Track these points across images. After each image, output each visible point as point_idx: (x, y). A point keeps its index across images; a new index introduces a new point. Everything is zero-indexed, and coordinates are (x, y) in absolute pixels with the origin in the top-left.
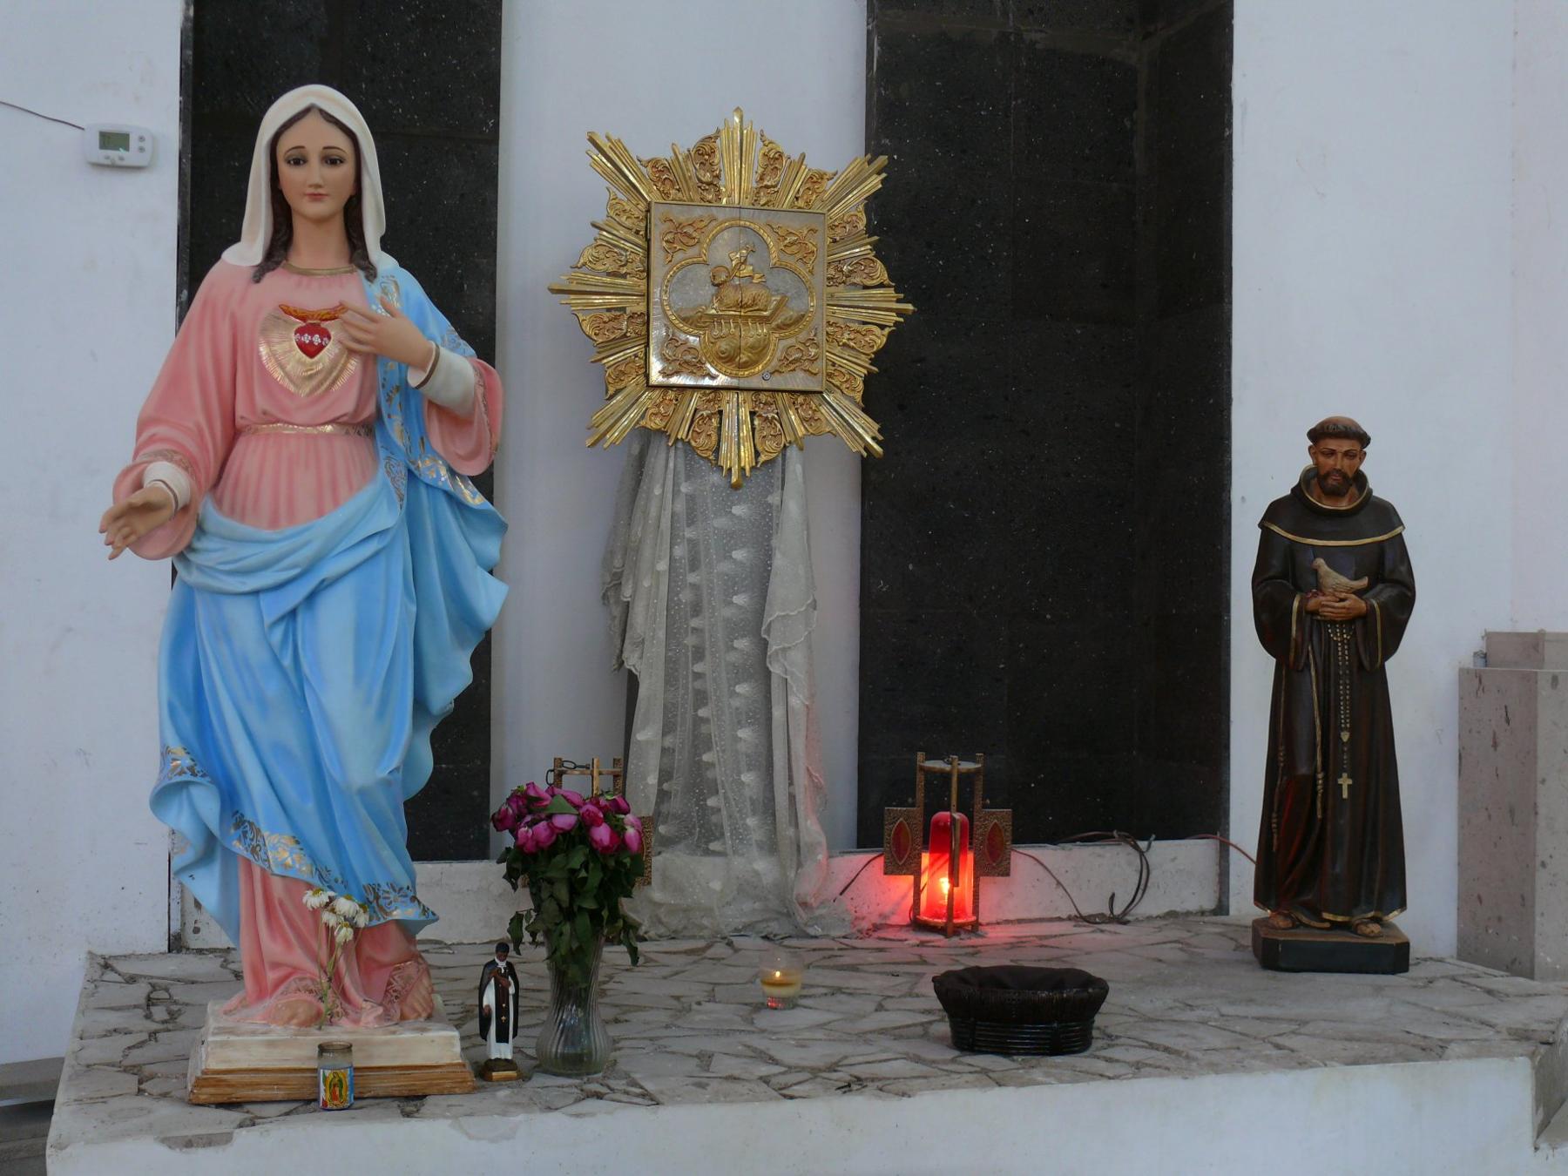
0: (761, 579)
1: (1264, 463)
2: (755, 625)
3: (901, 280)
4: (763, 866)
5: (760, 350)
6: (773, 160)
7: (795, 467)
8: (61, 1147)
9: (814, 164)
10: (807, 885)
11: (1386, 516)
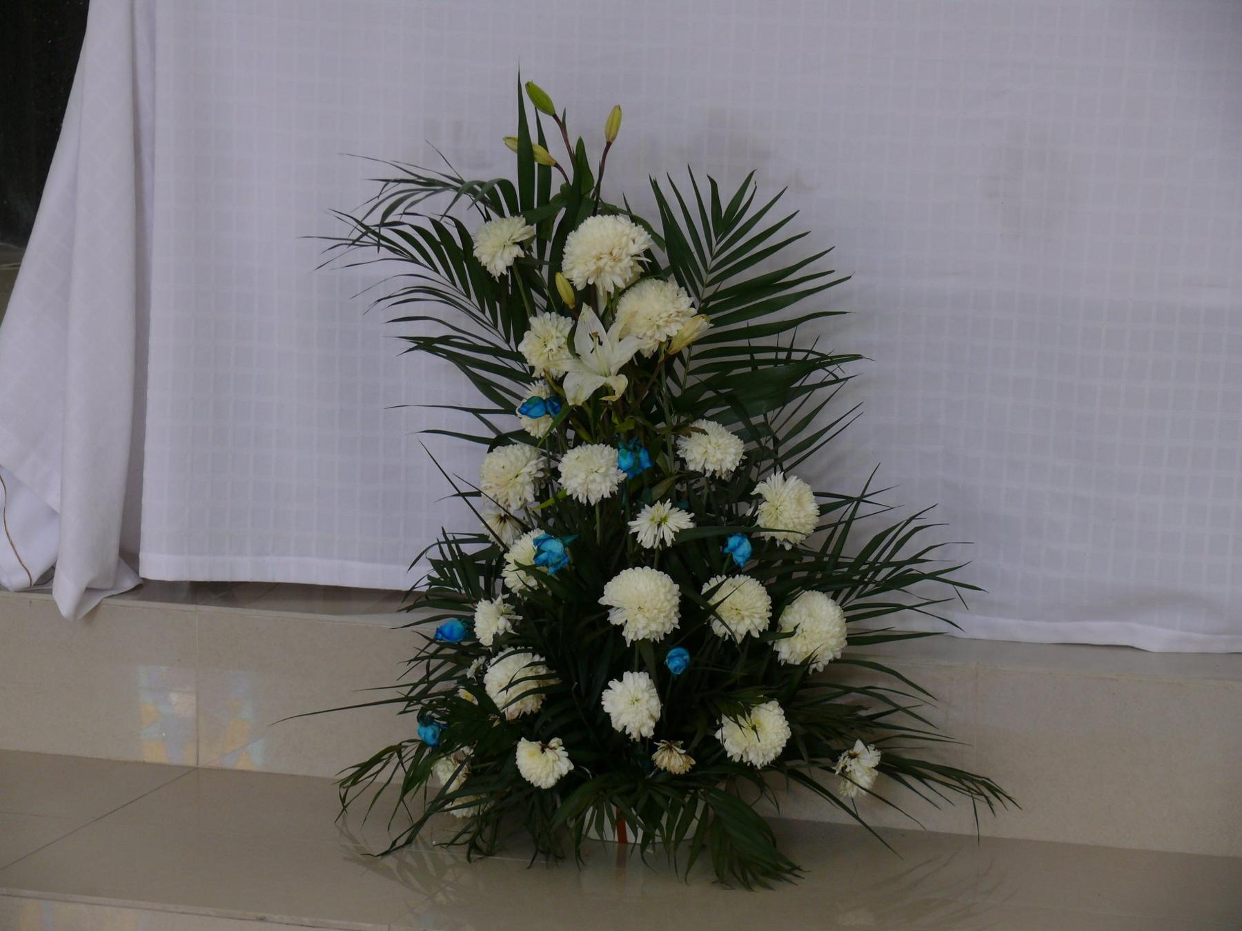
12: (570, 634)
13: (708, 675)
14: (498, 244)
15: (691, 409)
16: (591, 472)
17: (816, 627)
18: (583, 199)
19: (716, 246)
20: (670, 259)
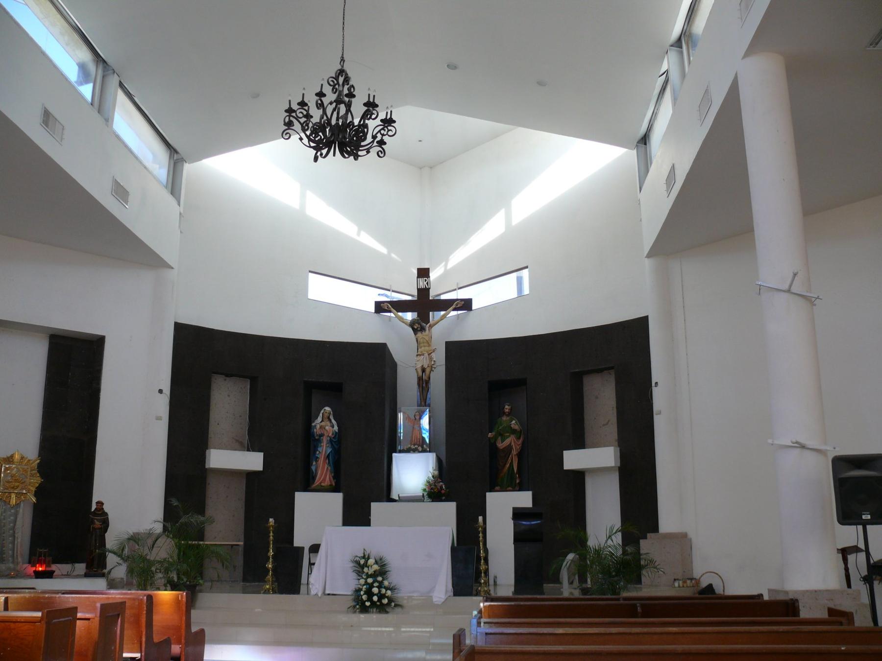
0: (15, 522)
1: (95, 499)
2: (14, 528)
3: (42, 476)
4: (11, 565)
5: (18, 487)
6: (22, 458)
7: (22, 505)
8: (659, 413)
9: (29, 458)
10: (18, 568)
11: (106, 514)
12: (369, 593)
13: (381, 597)
14: (362, 562)
15: (377, 576)
16: (370, 580)
17: (389, 593)
18: (369, 558)
19: (380, 562)
20: (376, 563)
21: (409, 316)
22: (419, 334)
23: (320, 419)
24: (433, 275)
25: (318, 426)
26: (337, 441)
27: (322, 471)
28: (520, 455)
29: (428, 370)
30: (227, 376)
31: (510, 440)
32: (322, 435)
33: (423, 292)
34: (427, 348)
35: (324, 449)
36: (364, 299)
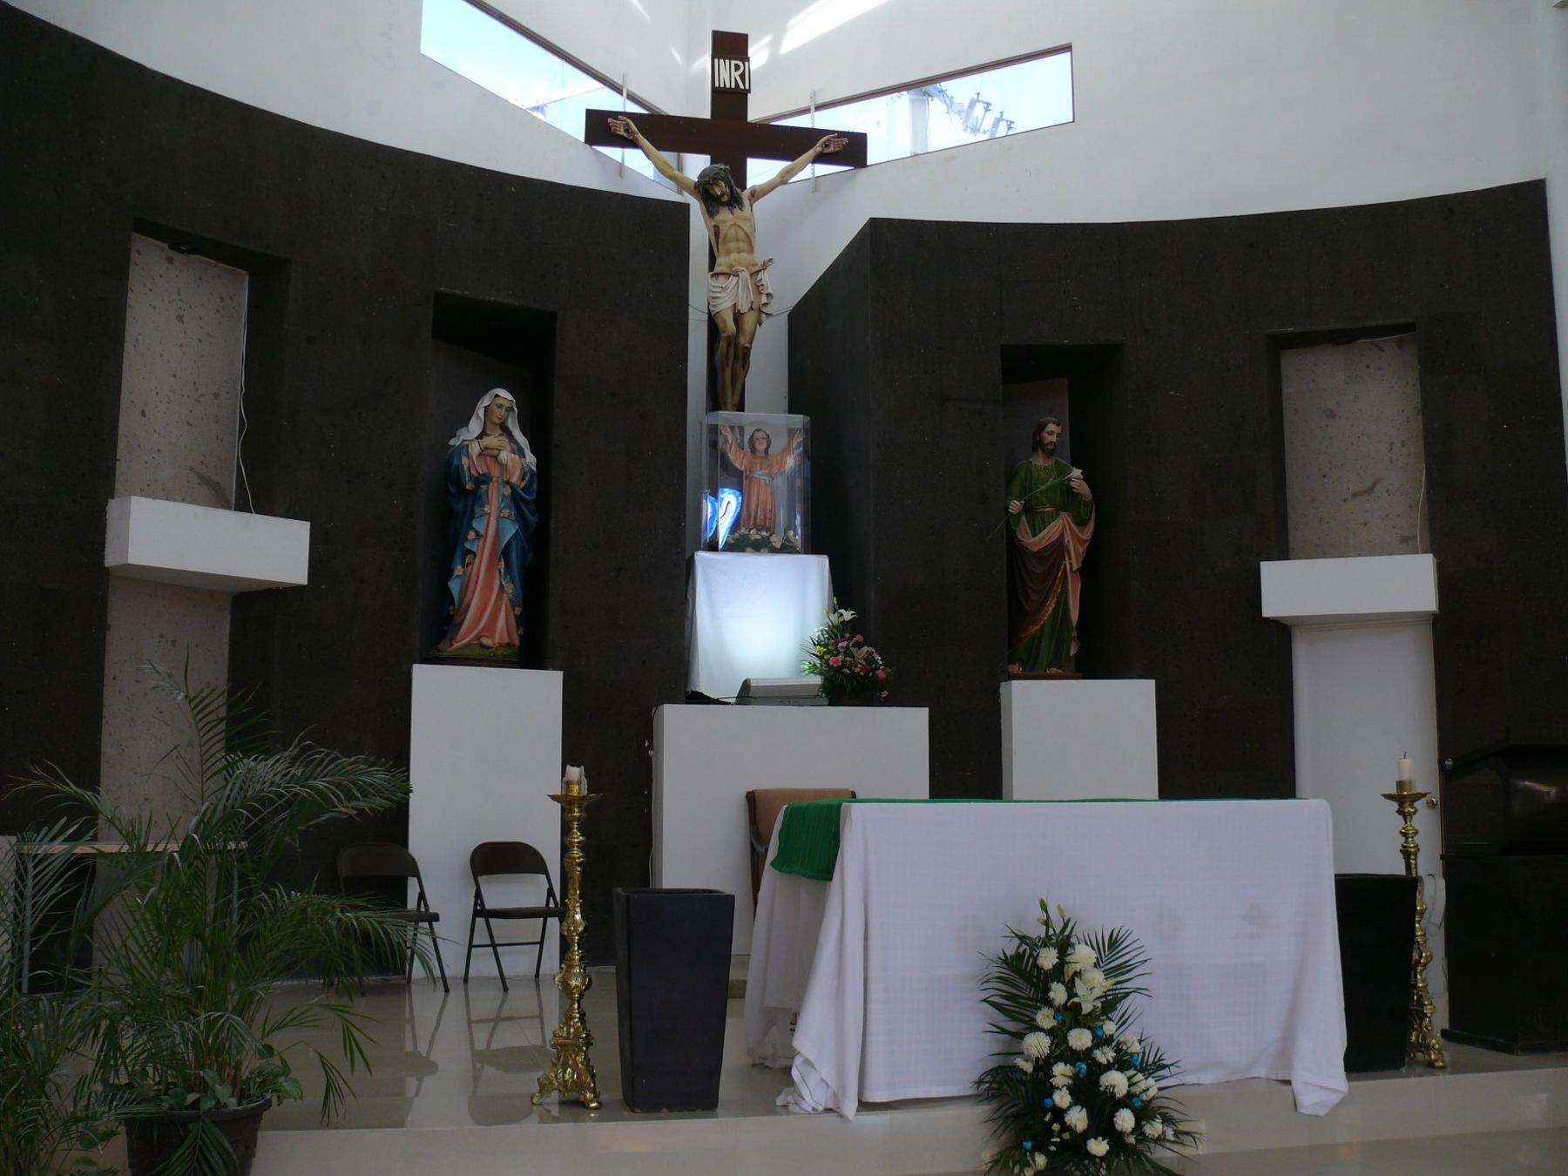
21: (696, 164)
22: (724, 215)
23: (475, 427)
24: (758, 55)
25: (475, 449)
26: (538, 503)
27: (486, 597)
28: (1088, 571)
29: (749, 320)
30: (175, 247)
31: (1058, 527)
32: (482, 480)
33: (730, 100)
34: (744, 256)
35: (494, 524)
36: (566, 100)
